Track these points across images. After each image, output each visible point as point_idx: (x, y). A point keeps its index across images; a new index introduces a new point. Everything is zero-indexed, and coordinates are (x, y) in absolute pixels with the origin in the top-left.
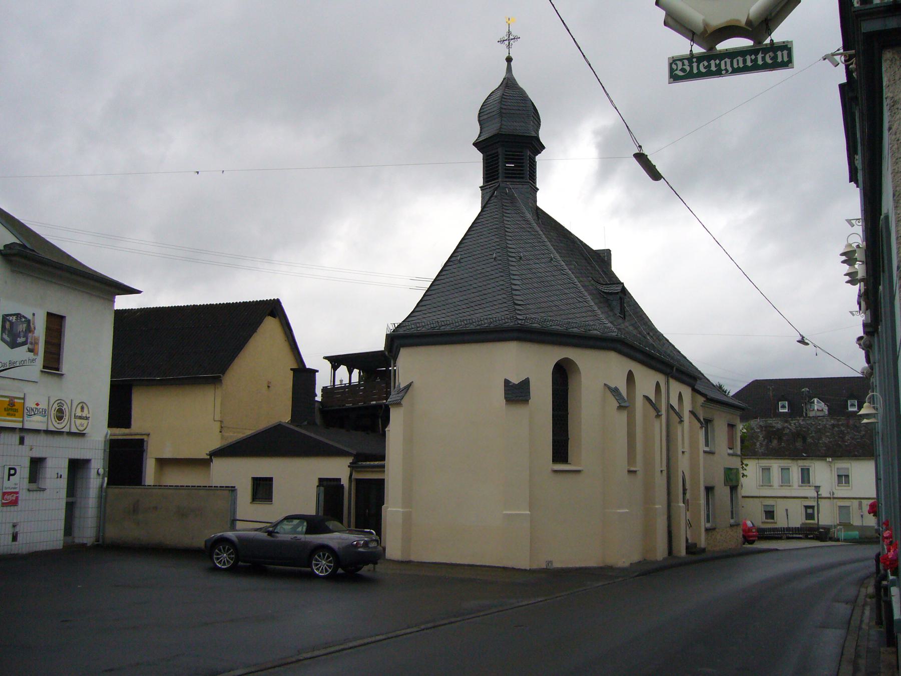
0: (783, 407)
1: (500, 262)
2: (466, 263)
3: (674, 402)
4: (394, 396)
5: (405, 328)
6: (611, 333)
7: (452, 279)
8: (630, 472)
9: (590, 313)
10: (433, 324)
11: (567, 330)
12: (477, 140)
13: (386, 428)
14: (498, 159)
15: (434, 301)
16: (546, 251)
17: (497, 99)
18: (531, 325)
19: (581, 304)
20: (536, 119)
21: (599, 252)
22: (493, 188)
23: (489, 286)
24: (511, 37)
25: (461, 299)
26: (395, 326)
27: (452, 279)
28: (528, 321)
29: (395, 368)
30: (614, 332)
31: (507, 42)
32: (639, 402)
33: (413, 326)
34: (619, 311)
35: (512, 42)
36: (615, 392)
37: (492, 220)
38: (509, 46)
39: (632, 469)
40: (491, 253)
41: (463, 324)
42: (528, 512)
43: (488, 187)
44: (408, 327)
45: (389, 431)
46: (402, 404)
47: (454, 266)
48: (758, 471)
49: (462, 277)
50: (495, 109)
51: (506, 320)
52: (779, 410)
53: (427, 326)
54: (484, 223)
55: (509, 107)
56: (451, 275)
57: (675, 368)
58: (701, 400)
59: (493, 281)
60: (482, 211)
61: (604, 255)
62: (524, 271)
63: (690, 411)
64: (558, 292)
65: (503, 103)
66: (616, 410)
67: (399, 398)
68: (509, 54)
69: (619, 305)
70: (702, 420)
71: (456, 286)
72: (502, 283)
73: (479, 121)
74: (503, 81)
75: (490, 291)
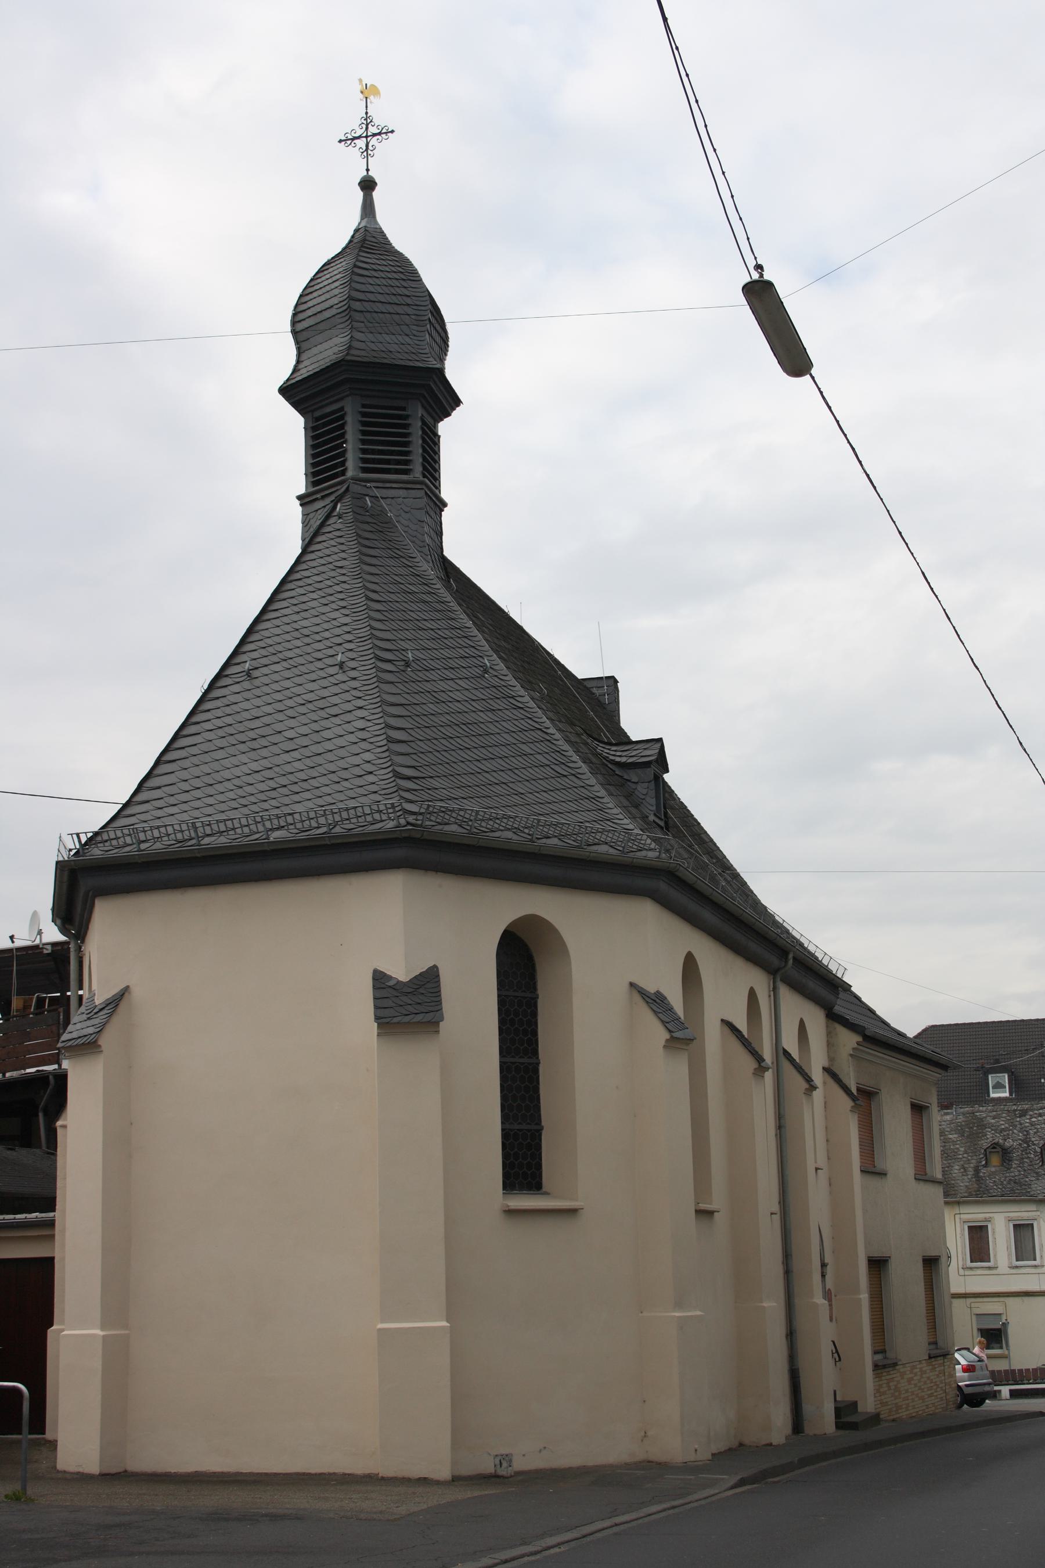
0: (999, 1086)
1: (353, 674)
2: (265, 680)
3: (790, 1043)
4: (79, 1026)
5: (107, 844)
6: (644, 853)
7: (229, 720)
8: (699, 1212)
9: (587, 804)
10: (182, 831)
11: (531, 841)
12: (288, 380)
13: (58, 1120)
14: (342, 426)
15: (184, 775)
16: (471, 652)
17: (338, 277)
18: (440, 827)
19: (564, 781)
20: (438, 328)
21: (589, 685)
22: (332, 498)
23: (327, 734)
24: (372, 130)
25: (255, 766)
26: (80, 841)
27: (229, 720)
28: (433, 818)
29: (81, 992)
30: (651, 850)
31: (361, 143)
32: (713, 1036)
33: (128, 840)
34: (654, 808)
35: (373, 141)
36: (657, 1002)
37: (333, 574)
38: (367, 151)
39: (703, 1206)
40: (331, 652)
41: (261, 828)
42: (445, 1324)
43: (318, 496)
44: (114, 843)
45: (64, 1127)
46: (100, 1046)
47: (236, 688)
48: (958, 1229)
49: (256, 713)
50: (335, 300)
51: (377, 816)
52: (989, 1096)
53: (166, 838)
54: (309, 581)
55: (371, 297)
56: (228, 710)
57: (791, 956)
58: (849, 1040)
59: (337, 721)
60: (305, 551)
61: (600, 691)
62: (416, 696)
63: (824, 1068)
64: (505, 751)
65: (354, 285)
66: (661, 1050)
67: (91, 1030)
68: (368, 170)
69: (653, 793)
70: (854, 1091)
71: (241, 737)
72: (361, 724)
73: (294, 333)
74: (353, 237)
75: (329, 745)
